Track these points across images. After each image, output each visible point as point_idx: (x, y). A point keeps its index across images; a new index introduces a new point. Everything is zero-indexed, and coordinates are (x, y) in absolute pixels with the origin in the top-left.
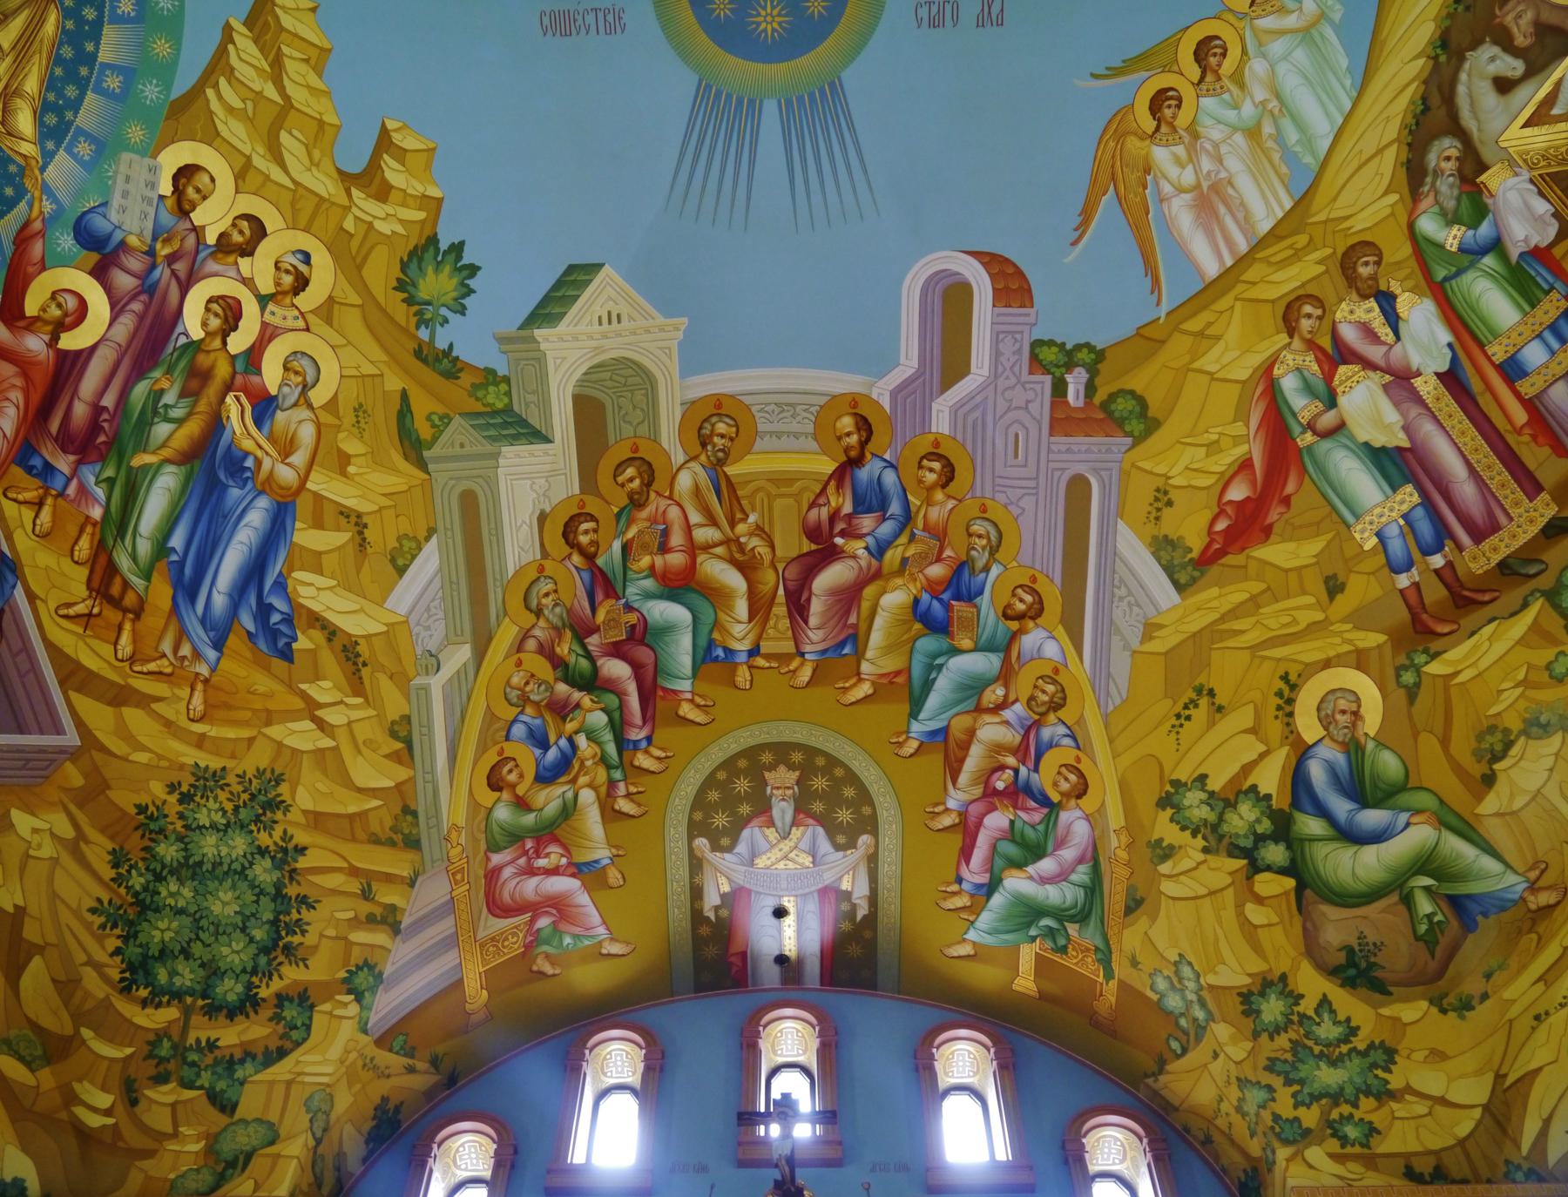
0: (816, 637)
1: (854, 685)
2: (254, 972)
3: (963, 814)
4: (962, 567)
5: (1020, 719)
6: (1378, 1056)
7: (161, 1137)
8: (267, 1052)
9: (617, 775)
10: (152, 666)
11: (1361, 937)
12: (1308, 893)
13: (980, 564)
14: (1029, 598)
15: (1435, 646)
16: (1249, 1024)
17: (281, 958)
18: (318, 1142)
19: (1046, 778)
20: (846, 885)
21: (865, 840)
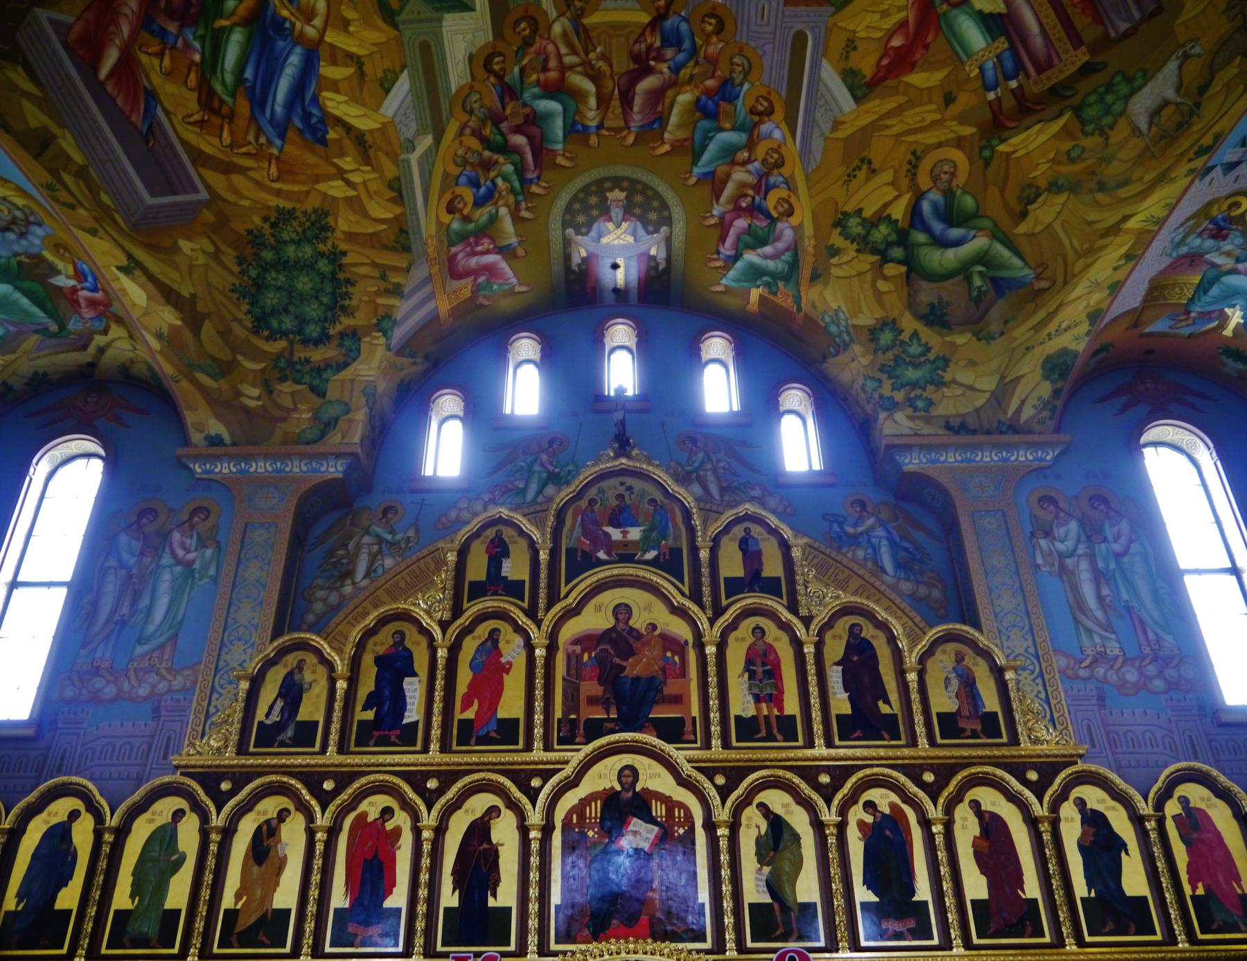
0: (637, 118)
1: (659, 146)
2: (325, 320)
3: (722, 217)
4: (726, 83)
5: (756, 169)
6: (940, 363)
7: (289, 411)
8: (338, 364)
9: (520, 198)
10: (244, 150)
11: (940, 298)
12: (913, 275)
13: (738, 81)
14: (766, 104)
15: (1005, 135)
16: (872, 346)
17: (339, 313)
18: (371, 410)
19: (771, 202)
20: (653, 252)
21: (664, 229)
